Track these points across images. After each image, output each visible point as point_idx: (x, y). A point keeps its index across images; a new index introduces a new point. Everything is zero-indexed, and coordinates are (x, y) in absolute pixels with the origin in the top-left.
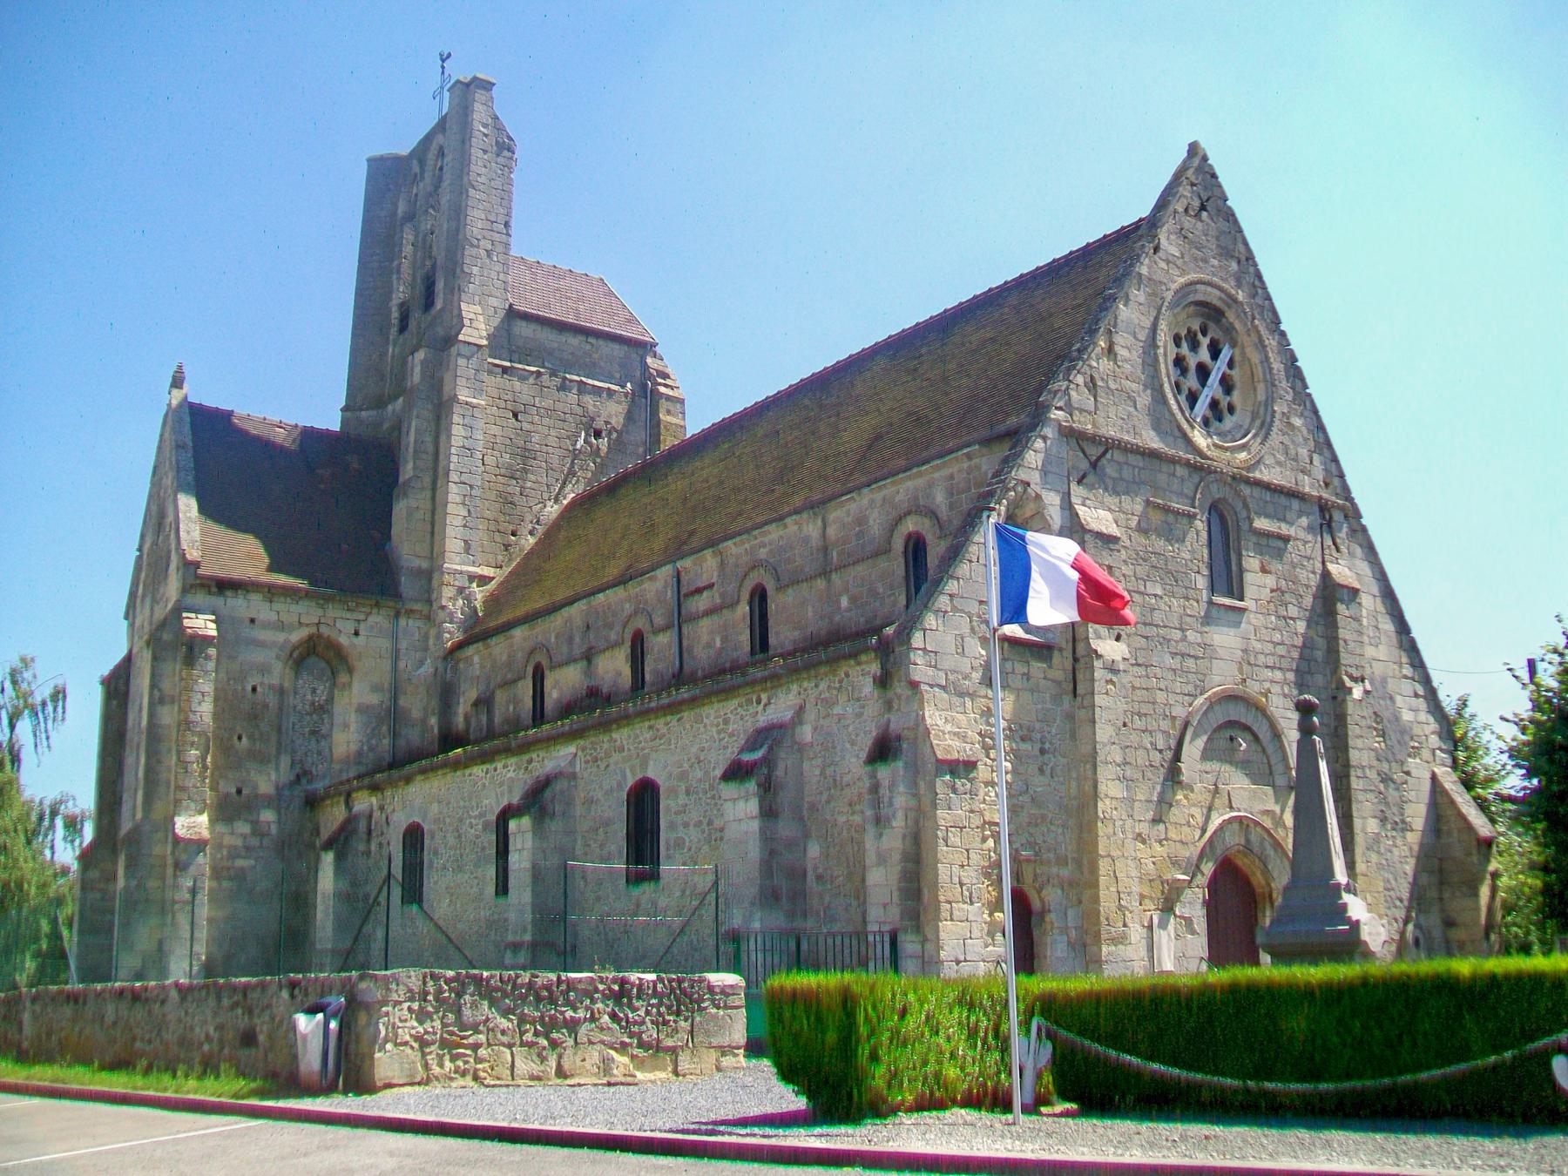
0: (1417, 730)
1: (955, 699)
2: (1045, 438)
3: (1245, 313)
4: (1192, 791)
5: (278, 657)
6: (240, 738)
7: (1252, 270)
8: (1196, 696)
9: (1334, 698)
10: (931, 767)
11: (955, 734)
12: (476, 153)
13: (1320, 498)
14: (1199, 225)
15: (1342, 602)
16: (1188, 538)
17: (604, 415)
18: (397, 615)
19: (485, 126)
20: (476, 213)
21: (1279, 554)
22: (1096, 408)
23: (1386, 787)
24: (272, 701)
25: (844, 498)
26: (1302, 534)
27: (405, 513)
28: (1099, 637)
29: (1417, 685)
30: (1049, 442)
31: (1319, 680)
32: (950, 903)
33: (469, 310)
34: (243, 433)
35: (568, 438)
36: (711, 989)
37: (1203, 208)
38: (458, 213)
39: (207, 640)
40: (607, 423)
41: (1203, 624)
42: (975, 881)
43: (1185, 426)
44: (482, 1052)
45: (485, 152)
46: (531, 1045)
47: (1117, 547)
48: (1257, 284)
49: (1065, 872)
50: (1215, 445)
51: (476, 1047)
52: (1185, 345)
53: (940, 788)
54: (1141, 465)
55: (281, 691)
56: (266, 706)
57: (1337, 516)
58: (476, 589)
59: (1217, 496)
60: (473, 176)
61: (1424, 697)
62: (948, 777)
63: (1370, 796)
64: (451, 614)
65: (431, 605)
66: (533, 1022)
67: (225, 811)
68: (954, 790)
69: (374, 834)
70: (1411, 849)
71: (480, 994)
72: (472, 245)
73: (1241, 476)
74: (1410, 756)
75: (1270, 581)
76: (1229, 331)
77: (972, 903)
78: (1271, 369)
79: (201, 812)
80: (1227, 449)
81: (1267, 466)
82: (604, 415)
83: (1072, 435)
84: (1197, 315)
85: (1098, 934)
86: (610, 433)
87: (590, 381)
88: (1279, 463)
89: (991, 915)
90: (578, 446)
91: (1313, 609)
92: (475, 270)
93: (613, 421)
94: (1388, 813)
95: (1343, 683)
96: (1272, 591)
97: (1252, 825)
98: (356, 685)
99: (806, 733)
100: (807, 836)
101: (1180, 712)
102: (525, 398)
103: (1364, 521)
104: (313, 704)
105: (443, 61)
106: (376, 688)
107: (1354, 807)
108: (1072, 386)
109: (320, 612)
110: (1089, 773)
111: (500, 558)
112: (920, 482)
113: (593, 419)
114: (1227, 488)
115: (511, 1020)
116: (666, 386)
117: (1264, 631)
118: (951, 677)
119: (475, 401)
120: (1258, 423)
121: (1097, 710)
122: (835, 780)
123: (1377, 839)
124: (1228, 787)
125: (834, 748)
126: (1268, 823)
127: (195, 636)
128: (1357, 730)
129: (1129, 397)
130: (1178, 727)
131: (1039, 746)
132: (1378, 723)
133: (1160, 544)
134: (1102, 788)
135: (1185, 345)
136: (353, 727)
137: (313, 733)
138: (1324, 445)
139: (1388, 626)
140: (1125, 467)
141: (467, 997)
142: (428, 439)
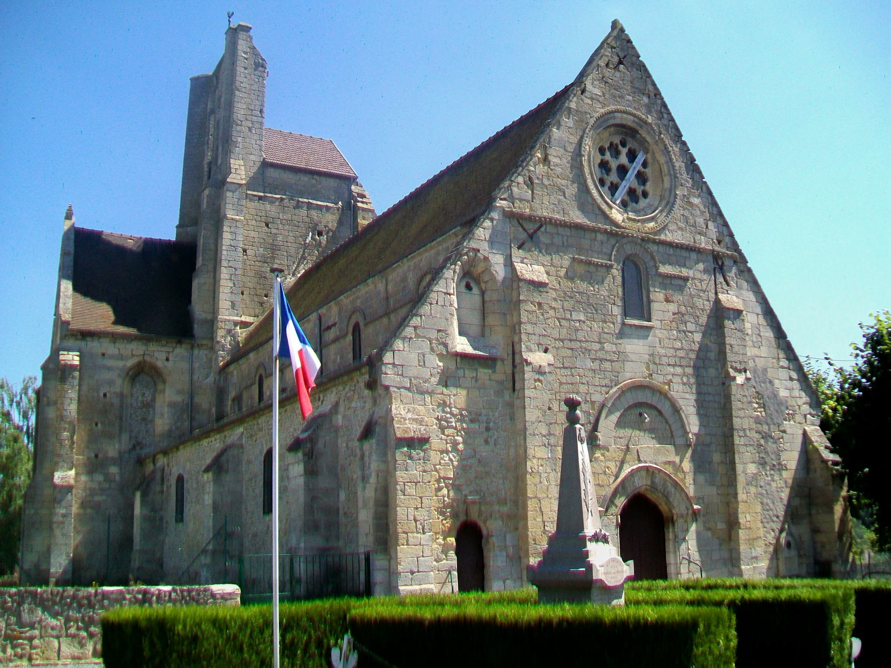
0: (791, 402)
1: (417, 396)
2: (492, 220)
3: (654, 130)
4: (608, 451)
5: (119, 375)
6: (97, 424)
7: (659, 101)
8: (612, 387)
9: (724, 384)
10: (393, 443)
11: (414, 420)
12: (240, 69)
13: (713, 251)
14: (618, 74)
15: (729, 319)
16: (607, 281)
17: (324, 222)
18: (192, 347)
19: (245, 53)
20: (239, 105)
21: (681, 289)
22: (533, 198)
23: (766, 442)
24: (116, 401)
25: (395, 265)
26: (698, 275)
27: (199, 284)
28: (530, 350)
29: (792, 372)
30: (495, 222)
31: (712, 372)
32: (406, 533)
33: (235, 163)
34: (108, 244)
35: (301, 236)
36: (213, 595)
37: (620, 62)
38: (230, 105)
39: (73, 367)
40: (325, 226)
41: (617, 338)
42: (426, 518)
43: (604, 207)
44: (36, 642)
45: (246, 68)
46: (73, 636)
47: (545, 289)
48: (663, 110)
49: (505, 509)
50: (629, 219)
51: (31, 639)
52: (608, 154)
53: (399, 456)
54: (569, 234)
55: (122, 396)
56: (112, 404)
57: (728, 262)
58: (239, 331)
59: (630, 253)
60: (238, 84)
61: (798, 380)
62: (406, 449)
63: (750, 448)
64: (223, 346)
65: (213, 341)
66: (76, 621)
67: (94, 465)
68: (411, 458)
69: (165, 481)
70: (786, 482)
71: (35, 603)
72: (237, 125)
73: (649, 238)
74: (785, 420)
75: (673, 307)
76: (643, 143)
77: (424, 533)
78: (674, 166)
79: (71, 469)
80: (638, 221)
81: (671, 231)
82: (324, 222)
83: (510, 216)
84: (617, 133)
85: (527, 551)
86: (328, 232)
87: (315, 202)
88: (681, 229)
89: (444, 539)
90: (307, 241)
91: (707, 325)
92: (239, 139)
93: (330, 225)
94: (768, 460)
95: (728, 373)
96: (674, 314)
97: (656, 472)
98: (168, 392)
99: (339, 419)
100: (339, 486)
101: (598, 398)
102: (273, 214)
103: (749, 265)
104: (143, 401)
105: (230, 17)
106: (179, 392)
107: (737, 456)
108: (514, 184)
109: (144, 348)
110: (522, 442)
111: (257, 311)
112: (433, 252)
113: (317, 225)
114: (638, 247)
115: (59, 620)
116: (363, 202)
117: (666, 341)
118: (414, 381)
119: (237, 217)
120: (664, 203)
121: (527, 400)
122: (352, 450)
123: (755, 477)
124: (638, 447)
125: (352, 429)
126: (669, 470)
127: (66, 365)
128: (739, 405)
129: (560, 189)
130: (596, 408)
131: (485, 425)
132: (760, 399)
133: (583, 286)
134: (530, 452)
135: (608, 154)
136: (166, 416)
137: (144, 419)
138: (716, 214)
139: (768, 334)
140: (555, 236)
141: (26, 606)
142: (212, 241)
